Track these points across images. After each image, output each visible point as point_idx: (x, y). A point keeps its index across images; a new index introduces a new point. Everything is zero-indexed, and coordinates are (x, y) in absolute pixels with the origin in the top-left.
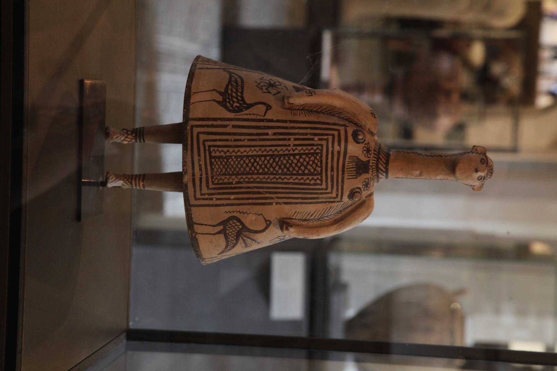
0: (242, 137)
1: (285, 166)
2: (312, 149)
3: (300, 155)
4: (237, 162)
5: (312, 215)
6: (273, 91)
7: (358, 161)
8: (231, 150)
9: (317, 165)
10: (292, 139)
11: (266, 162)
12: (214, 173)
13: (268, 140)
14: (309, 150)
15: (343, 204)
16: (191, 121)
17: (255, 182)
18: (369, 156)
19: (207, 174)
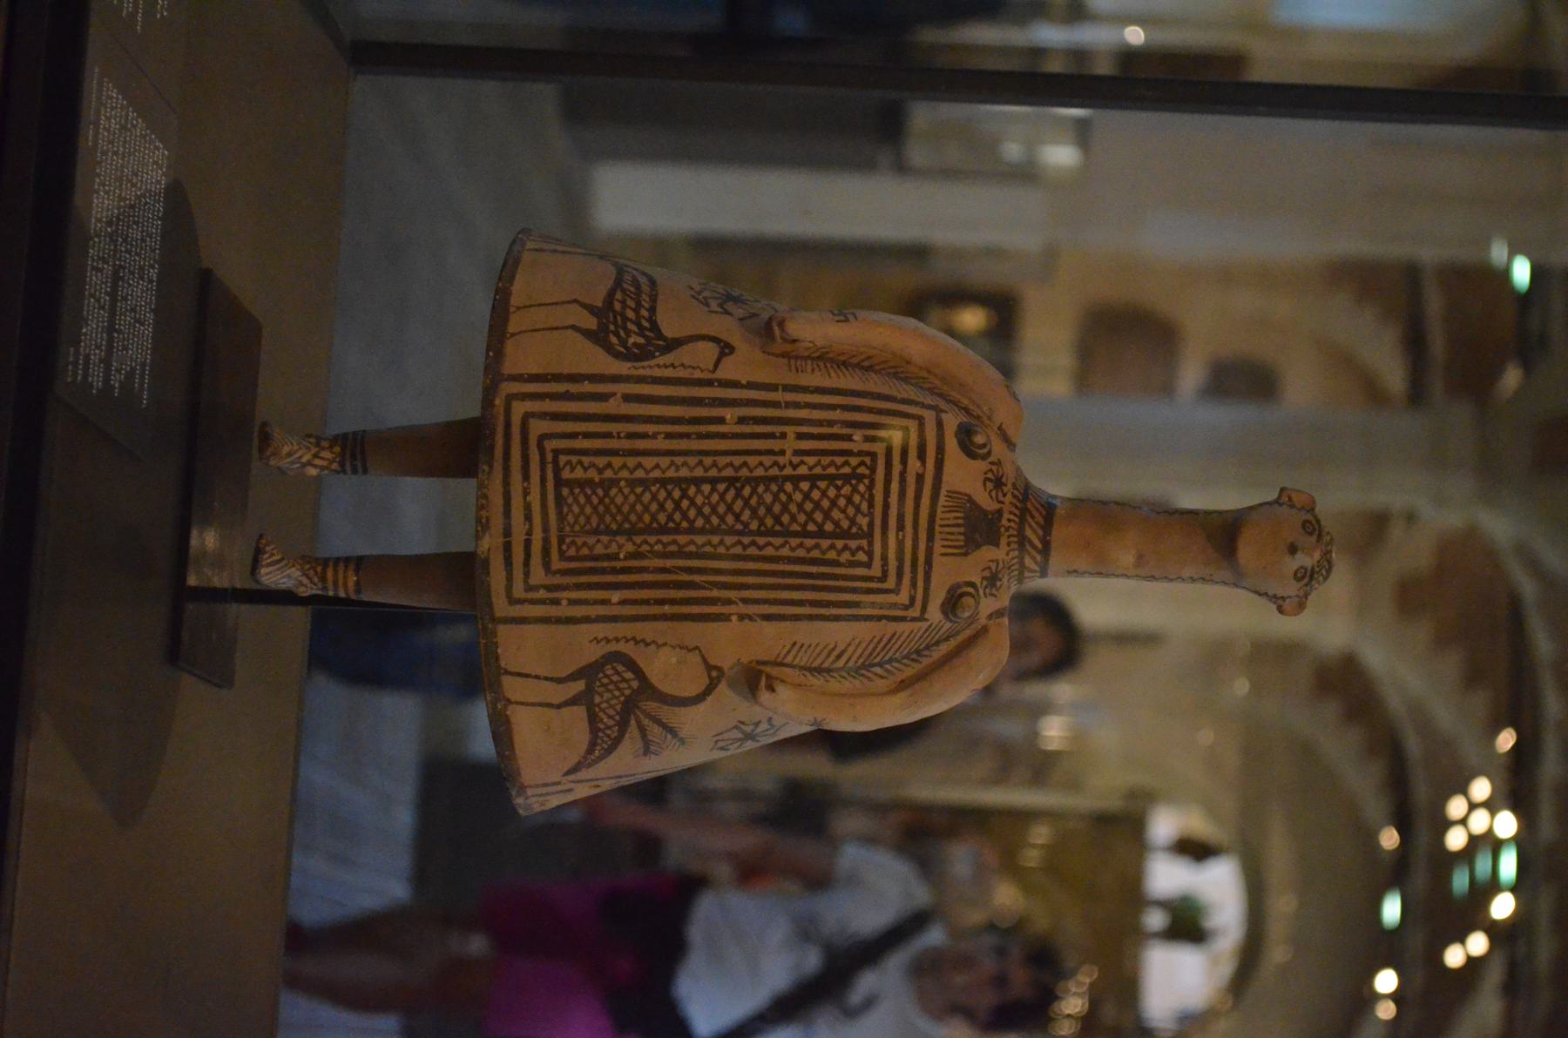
0: (651, 429)
1: (769, 510)
2: (846, 463)
3: (813, 479)
4: (632, 498)
5: (839, 657)
6: (739, 312)
7: (970, 506)
8: (617, 462)
9: (858, 509)
10: (791, 436)
11: (715, 497)
12: (568, 529)
13: (724, 436)
14: (838, 468)
15: (927, 630)
16: (506, 383)
17: (681, 554)
18: (1001, 498)
19: (546, 530)
